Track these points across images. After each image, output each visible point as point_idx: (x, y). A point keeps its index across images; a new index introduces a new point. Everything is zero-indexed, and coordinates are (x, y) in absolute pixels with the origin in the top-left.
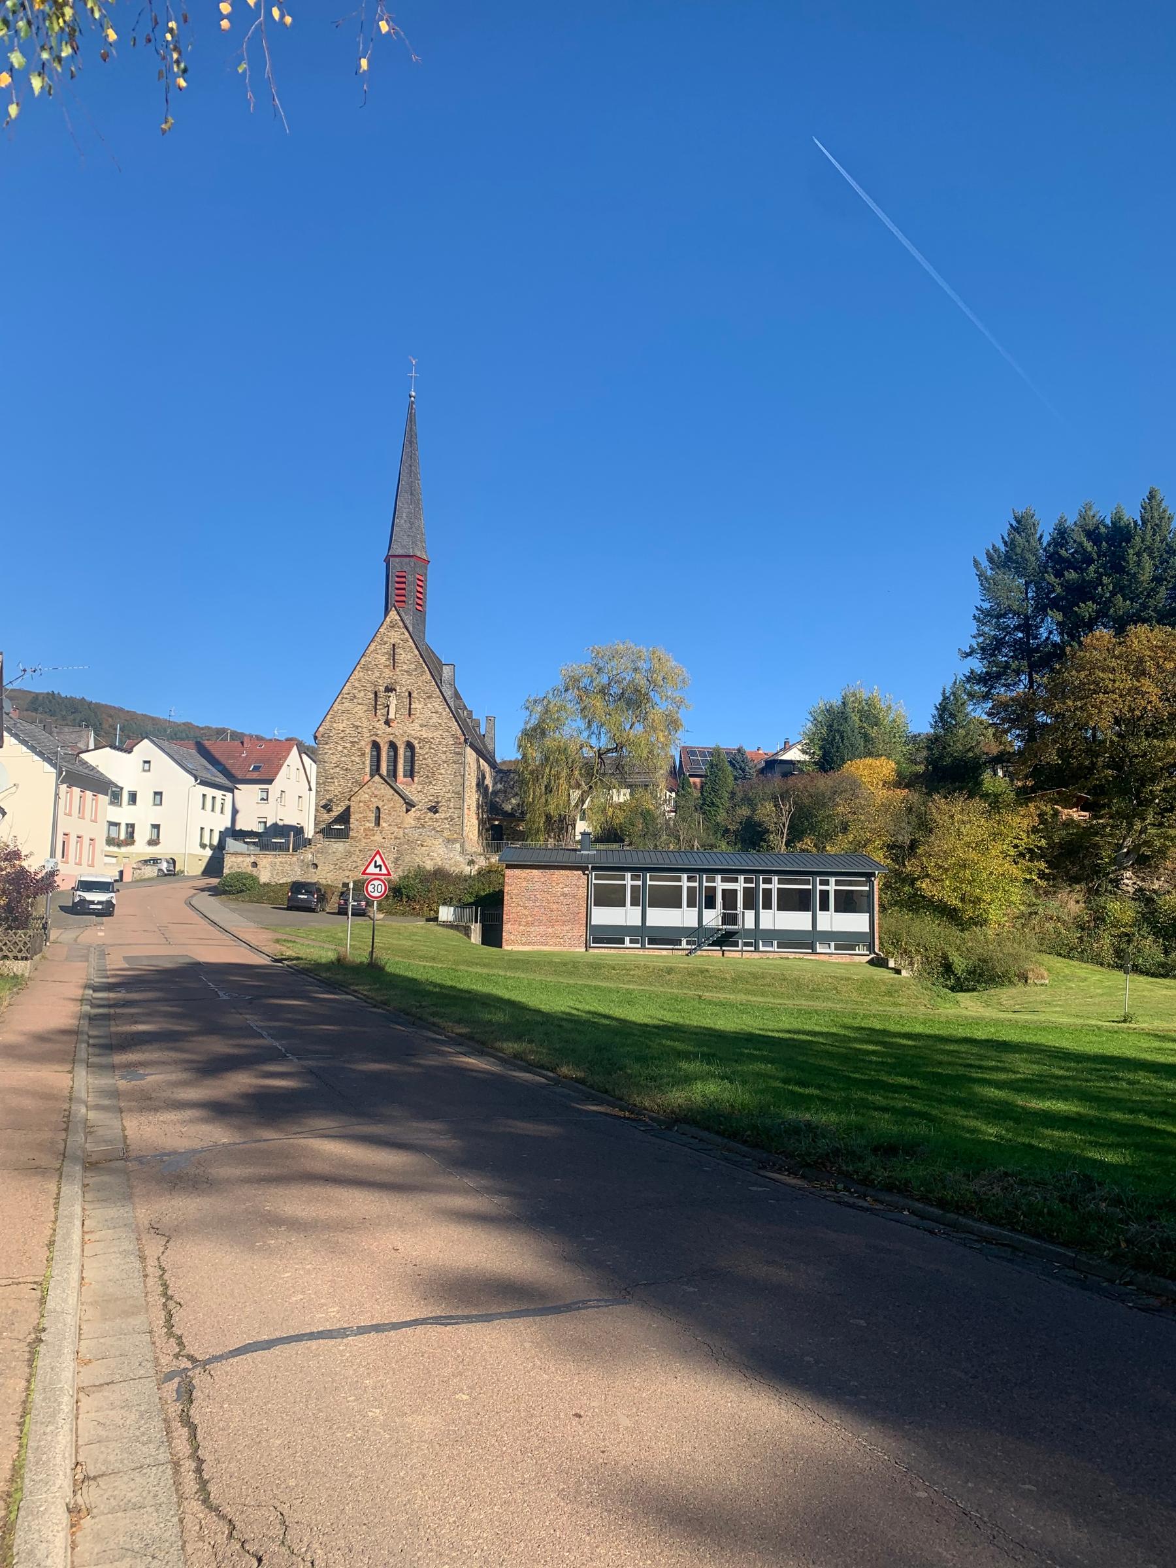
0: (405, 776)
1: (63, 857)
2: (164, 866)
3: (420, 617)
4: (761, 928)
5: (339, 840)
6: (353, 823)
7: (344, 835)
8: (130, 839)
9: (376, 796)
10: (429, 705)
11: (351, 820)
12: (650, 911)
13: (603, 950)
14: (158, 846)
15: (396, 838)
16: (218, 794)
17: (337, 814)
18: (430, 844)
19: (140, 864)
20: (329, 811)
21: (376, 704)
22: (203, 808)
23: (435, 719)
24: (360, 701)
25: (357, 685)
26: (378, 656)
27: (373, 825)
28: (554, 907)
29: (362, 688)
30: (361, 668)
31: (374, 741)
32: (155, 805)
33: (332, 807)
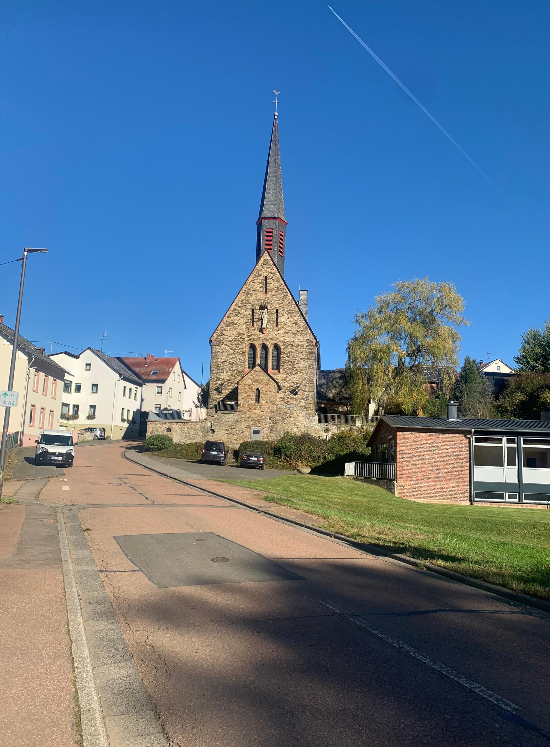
0: (273, 369)
1: (30, 422)
2: (98, 433)
3: (281, 260)
4: (524, 482)
5: (230, 412)
6: (240, 401)
7: (233, 408)
8: (76, 415)
9: (257, 381)
10: (291, 319)
11: (239, 398)
12: (526, 471)
13: (486, 505)
14: (94, 420)
15: (271, 411)
16: (133, 386)
17: (225, 395)
18: (296, 416)
19: (83, 431)
20: (220, 393)
21: (253, 318)
22: (124, 395)
23: (295, 328)
24: (242, 316)
25: (240, 305)
26: (255, 285)
27: (255, 402)
28: (441, 465)
29: (244, 307)
30: (243, 293)
31: (252, 343)
32: (93, 392)
33: (222, 389)
